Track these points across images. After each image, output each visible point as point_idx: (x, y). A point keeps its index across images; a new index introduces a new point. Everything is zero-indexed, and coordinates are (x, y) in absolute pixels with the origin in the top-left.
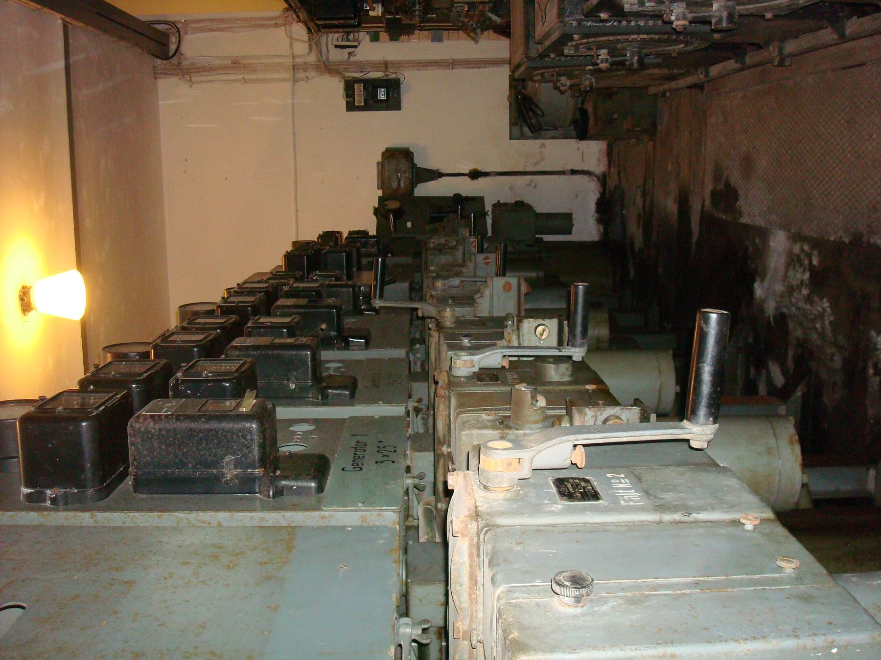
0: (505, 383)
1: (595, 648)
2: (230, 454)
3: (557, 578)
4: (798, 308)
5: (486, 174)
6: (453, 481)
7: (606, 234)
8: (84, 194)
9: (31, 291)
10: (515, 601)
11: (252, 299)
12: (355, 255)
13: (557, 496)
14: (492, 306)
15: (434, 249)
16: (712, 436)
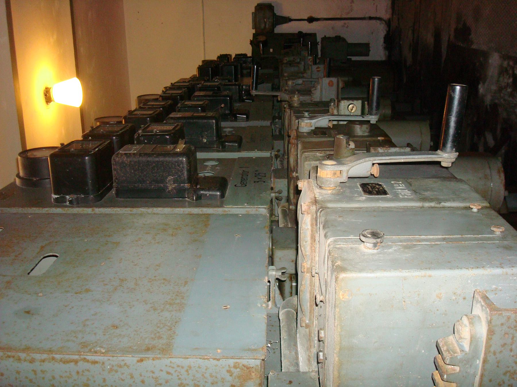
0: (330, 136)
1: (385, 270)
2: (171, 175)
3: (364, 233)
4: (504, 100)
5: (317, 20)
6: (301, 185)
7: (389, 56)
8: (79, 33)
9: (51, 91)
10: (338, 246)
11: (180, 92)
12: (239, 68)
13: (362, 193)
14: (321, 95)
15: (286, 63)
16: (454, 160)
